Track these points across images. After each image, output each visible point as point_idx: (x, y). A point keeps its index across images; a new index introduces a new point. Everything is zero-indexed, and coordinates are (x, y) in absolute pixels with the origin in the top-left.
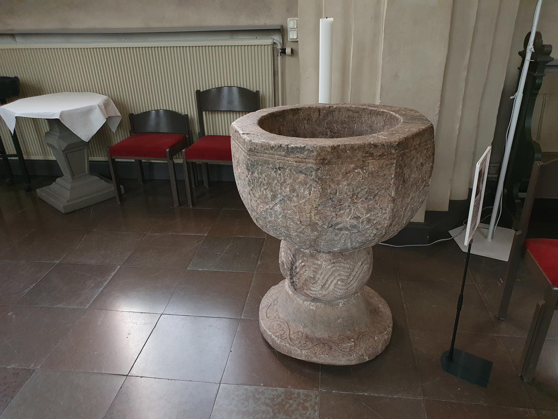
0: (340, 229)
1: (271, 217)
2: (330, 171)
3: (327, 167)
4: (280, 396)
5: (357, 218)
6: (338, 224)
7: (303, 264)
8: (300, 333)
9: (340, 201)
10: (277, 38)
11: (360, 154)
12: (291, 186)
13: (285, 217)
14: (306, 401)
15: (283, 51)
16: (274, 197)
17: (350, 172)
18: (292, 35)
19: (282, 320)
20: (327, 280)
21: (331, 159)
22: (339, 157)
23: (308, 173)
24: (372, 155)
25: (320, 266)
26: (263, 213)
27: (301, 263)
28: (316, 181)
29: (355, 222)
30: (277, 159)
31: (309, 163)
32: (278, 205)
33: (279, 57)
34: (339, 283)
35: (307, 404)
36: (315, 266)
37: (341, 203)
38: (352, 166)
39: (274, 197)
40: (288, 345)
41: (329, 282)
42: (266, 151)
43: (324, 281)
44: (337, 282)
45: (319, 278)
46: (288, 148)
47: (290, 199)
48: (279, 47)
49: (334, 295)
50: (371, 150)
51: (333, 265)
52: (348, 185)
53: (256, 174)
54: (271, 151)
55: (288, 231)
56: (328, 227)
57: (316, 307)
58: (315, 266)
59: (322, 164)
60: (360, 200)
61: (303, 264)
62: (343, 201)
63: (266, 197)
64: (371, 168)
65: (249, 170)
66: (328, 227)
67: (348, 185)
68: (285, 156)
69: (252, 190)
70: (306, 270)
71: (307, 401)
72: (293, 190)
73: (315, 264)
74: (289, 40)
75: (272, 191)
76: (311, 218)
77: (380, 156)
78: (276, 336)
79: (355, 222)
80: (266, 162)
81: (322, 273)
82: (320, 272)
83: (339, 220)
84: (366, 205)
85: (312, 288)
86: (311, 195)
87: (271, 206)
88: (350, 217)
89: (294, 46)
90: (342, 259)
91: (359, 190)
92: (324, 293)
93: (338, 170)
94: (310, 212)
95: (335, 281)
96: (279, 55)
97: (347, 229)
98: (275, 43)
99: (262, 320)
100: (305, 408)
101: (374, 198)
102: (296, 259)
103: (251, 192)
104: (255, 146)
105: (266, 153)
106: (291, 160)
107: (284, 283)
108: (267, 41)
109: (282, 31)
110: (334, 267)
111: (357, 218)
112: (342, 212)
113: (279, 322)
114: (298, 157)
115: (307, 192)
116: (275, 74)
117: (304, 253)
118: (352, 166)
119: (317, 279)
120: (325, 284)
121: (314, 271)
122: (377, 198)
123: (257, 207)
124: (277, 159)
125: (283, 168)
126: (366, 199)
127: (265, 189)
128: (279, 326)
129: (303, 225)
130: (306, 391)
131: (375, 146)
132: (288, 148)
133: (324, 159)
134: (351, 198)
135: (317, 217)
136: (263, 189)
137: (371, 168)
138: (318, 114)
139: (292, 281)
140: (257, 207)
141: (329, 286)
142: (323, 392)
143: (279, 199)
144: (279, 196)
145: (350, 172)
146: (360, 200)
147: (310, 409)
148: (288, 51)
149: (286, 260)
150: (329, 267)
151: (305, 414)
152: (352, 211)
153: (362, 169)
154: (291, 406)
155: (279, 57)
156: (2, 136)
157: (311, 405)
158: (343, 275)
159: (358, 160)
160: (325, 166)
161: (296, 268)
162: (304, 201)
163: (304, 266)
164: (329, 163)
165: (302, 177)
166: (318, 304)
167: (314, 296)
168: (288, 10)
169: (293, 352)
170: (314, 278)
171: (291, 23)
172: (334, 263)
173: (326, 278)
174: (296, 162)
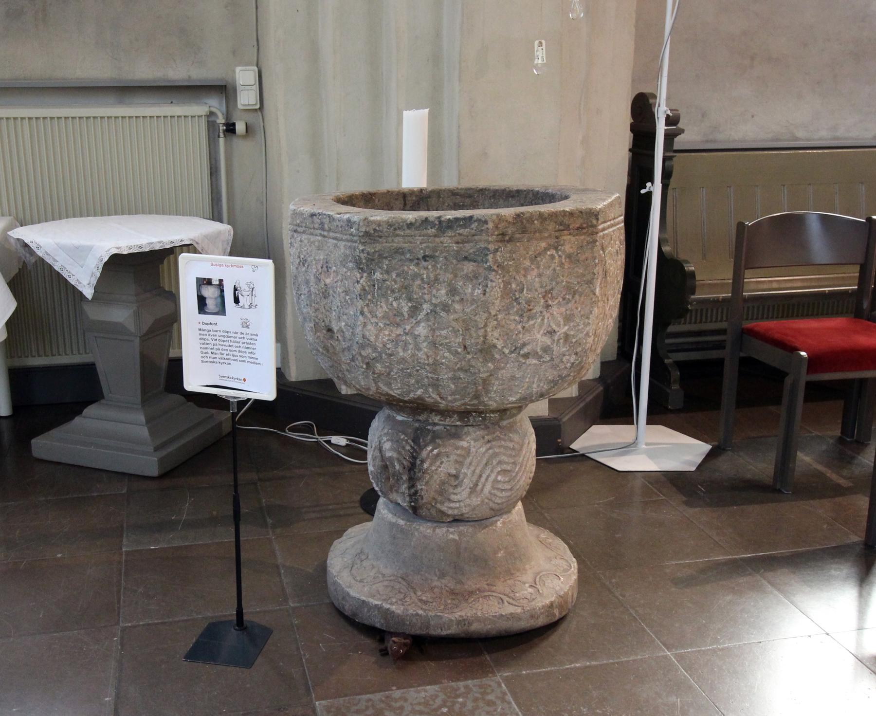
0: (526, 356)
1: (404, 350)
2: (514, 253)
3: (509, 247)
4: (437, 696)
5: (551, 333)
6: (524, 345)
7: (436, 451)
8: (436, 590)
9: (528, 302)
10: (215, 104)
11: (551, 226)
12: (449, 285)
13: (434, 345)
14: (484, 693)
15: (230, 129)
16: (415, 310)
17: (540, 254)
18: (246, 98)
19: (392, 578)
20: (480, 476)
21: (513, 233)
22: (524, 231)
23: (479, 259)
24: (567, 227)
25: (468, 451)
26: (388, 346)
27: (432, 450)
28: (494, 270)
29: (547, 340)
30: (420, 243)
31: (481, 241)
32: (423, 324)
33: (222, 141)
34: (499, 478)
35: (491, 697)
36: (459, 452)
37: (531, 307)
38: (543, 245)
39: (415, 310)
40: (420, 612)
41: (483, 479)
42: (398, 232)
43: (474, 479)
44: (497, 477)
45: (466, 474)
46: (440, 222)
47: (446, 308)
48: (221, 120)
49: (491, 504)
50: (566, 220)
51: (488, 445)
52: (540, 275)
53: (378, 275)
54: (408, 232)
55: (434, 371)
56: (511, 352)
57: (461, 534)
58: (459, 452)
59: (502, 241)
60: (557, 301)
61: (436, 451)
62: (533, 304)
63: (398, 313)
64: (567, 248)
65: (362, 269)
66: (511, 352)
67: (540, 275)
68: (435, 236)
69: (367, 305)
70: (442, 463)
71: (488, 694)
72: (453, 291)
73: (457, 448)
74: (240, 107)
75: (410, 299)
76: (485, 336)
77: (578, 228)
78: (391, 604)
79: (547, 340)
80: (399, 251)
81: (470, 464)
82: (468, 460)
83: (527, 338)
84: (564, 309)
85: (453, 497)
86: (487, 295)
87: (408, 327)
88: (542, 332)
89: (251, 118)
90: (501, 433)
91: (554, 283)
92: (476, 501)
93: (525, 252)
94: (486, 326)
95: (493, 476)
96: (221, 135)
97: (535, 354)
98: (212, 114)
99: (350, 587)
100: (490, 703)
101: (573, 297)
102: (419, 445)
103: (366, 309)
104: (374, 226)
105: (397, 235)
106: (447, 240)
107: (379, 511)
108: (198, 109)
109: (224, 90)
110: (490, 448)
111: (551, 333)
112: (531, 322)
113: (386, 583)
114: (460, 234)
115: (478, 292)
116: (214, 171)
117: (434, 432)
118: (543, 245)
119: (461, 476)
120: (476, 485)
121: (456, 462)
122: (577, 297)
123: (377, 336)
124: (420, 243)
125: (432, 257)
126: (564, 299)
127: (396, 299)
128: (389, 589)
129: (468, 353)
130: (476, 682)
131: (571, 214)
132: (440, 222)
133: (503, 234)
134: (544, 297)
135: (496, 334)
136: (391, 299)
137: (567, 248)
138: (403, 202)
139: (413, 491)
140: (377, 336)
141: (484, 485)
142: (507, 676)
143: (424, 312)
144: (425, 306)
145: (540, 254)
146: (557, 301)
147: (498, 702)
148: (240, 127)
149: (399, 453)
150: (483, 450)
151: (495, 710)
152: (546, 320)
153: (556, 248)
154: (463, 705)
155: (222, 141)
156: (4, 193)
157: (497, 697)
158: (508, 463)
159: (550, 236)
160: (506, 246)
161: (423, 461)
162: (473, 307)
163: (438, 455)
164: (510, 240)
165: (469, 267)
166: (461, 528)
167: (456, 512)
168: (234, 53)
169: (432, 623)
170: (456, 477)
171: (244, 77)
172: (489, 441)
173: (478, 471)
174: (457, 243)
